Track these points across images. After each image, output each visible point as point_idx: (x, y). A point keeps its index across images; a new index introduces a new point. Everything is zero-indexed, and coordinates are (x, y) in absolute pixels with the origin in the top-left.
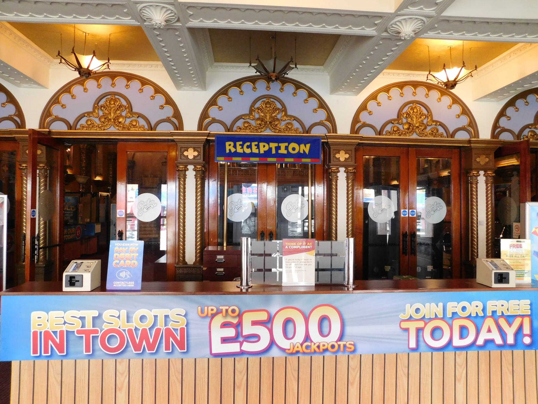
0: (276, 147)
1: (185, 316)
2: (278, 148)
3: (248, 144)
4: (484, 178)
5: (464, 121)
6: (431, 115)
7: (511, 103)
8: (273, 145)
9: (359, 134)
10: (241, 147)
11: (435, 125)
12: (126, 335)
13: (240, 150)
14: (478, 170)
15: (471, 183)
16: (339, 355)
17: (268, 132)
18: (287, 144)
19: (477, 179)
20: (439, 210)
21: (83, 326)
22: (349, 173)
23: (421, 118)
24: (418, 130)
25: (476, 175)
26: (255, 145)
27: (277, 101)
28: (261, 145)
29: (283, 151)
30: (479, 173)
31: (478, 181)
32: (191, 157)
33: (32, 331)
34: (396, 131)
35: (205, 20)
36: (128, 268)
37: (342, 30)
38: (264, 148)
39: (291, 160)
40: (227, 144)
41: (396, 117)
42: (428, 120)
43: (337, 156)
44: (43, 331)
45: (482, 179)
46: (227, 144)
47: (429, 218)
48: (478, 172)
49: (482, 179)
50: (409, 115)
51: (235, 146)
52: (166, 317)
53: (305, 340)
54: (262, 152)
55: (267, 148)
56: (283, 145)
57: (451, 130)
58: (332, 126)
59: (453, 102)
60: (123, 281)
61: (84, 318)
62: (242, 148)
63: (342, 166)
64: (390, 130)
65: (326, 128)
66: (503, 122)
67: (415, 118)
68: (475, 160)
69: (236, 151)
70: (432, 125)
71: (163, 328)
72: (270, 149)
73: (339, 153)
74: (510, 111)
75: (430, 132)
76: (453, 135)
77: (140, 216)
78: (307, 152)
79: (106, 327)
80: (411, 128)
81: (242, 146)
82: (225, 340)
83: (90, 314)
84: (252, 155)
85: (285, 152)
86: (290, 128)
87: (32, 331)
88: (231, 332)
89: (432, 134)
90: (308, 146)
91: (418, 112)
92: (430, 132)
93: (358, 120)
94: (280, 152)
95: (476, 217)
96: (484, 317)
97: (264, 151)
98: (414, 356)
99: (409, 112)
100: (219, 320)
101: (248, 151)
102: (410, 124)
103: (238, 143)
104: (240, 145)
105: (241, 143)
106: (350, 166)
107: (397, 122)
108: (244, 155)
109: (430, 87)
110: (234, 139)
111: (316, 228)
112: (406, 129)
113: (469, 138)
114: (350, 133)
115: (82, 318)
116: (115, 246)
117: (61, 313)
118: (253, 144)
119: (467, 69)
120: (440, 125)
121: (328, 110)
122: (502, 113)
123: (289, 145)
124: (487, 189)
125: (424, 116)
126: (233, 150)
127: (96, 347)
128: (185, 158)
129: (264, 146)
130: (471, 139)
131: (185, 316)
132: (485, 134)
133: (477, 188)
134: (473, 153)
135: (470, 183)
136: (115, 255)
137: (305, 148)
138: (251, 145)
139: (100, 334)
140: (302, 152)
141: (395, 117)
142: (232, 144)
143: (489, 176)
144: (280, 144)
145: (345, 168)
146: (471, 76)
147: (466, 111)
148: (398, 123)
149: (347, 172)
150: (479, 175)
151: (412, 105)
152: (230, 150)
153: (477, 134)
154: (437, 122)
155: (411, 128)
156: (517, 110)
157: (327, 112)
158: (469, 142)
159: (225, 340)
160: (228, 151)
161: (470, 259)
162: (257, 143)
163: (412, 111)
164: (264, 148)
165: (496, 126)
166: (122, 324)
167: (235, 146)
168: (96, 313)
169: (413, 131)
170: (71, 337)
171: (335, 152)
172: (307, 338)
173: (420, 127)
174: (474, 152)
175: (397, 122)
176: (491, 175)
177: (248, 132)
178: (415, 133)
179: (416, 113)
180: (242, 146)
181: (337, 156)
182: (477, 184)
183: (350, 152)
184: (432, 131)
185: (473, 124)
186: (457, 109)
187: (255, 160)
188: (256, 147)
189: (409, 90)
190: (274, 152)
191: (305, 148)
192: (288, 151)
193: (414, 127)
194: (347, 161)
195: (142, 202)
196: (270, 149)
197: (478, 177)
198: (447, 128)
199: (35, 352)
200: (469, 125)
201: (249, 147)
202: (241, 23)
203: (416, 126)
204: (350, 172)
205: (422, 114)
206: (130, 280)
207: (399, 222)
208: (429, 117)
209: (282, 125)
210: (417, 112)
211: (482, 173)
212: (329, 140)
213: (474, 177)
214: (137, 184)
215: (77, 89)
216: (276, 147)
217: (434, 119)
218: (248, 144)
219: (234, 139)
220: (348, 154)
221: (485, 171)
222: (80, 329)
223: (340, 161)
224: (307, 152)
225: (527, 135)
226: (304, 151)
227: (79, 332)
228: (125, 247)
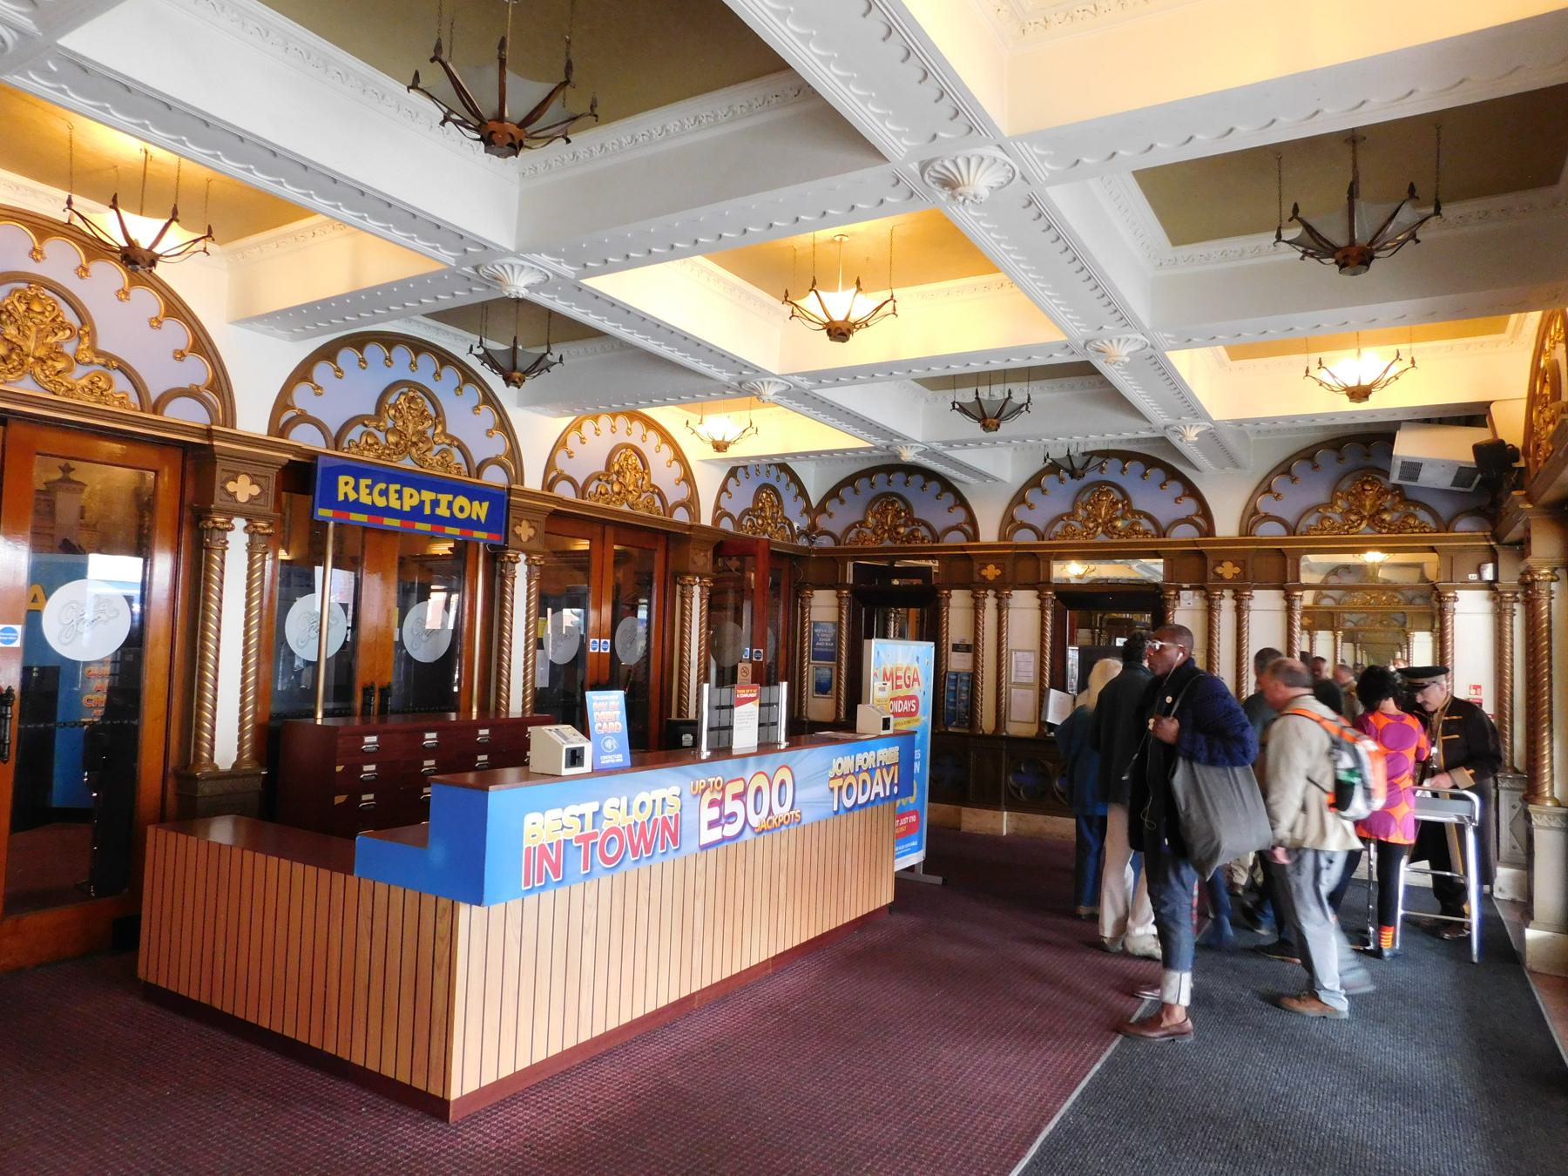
0: (432, 501)
1: (680, 797)
2: (435, 503)
3: (382, 486)
4: (246, 538)
5: (196, 372)
6: (92, 334)
7: (327, 353)
8: (428, 496)
9: (287, 439)
10: (368, 491)
11: (449, 445)
12: (625, 834)
13: (365, 499)
14: (230, 514)
15: (209, 549)
16: (791, 827)
17: (407, 464)
18: (450, 497)
19: (224, 538)
20: (105, 622)
21: (582, 830)
22: (257, 537)
23: (56, 334)
24: (43, 370)
25: (221, 527)
26: (396, 491)
27: (63, 299)
28: (407, 491)
29: (443, 511)
30: (233, 522)
31: (227, 542)
32: (242, 498)
33: (525, 847)
34: (371, 445)
35: (191, 143)
36: (613, 734)
37: (606, 326)
38: (411, 498)
39: (362, 518)
40: (342, 479)
41: (371, 411)
42: (82, 347)
43: (231, 486)
44: (537, 846)
45: (521, 569)
46: (342, 479)
47: (71, 642)
48: (229, 522)
49: (521, 569)
50: (400, 412)
51: (356, 489)
52: (664, 799)
53: (769, 815)
54: (407, 508)
55: (415, 502)
56: (444, 498)
57: (155, 392)
58: (224, 407)
59: (167, 310)
60: (611, 754)
61: (584, 815)
62: (371, 494)
63: (240, 514)
64: (357, 440)
65: (208, 409)
66: (303, 397)
67: (34, 329)
68: (224, 488)
69: (358, 499)
70: (91, 363)
71: (660, 817)
72: (422, 502)
73: (236, 481)
74: (322, 371)
75: (84, 382)
76: (157, 407)
77: (66, 644)
78: (483, 519)
79: (606, 826)
80: (14, 357)
81: (371, 488)
82: (712, 825)
83: (589, 808)
84: (389, 512)
85: (447, 514)
86: (105, 390)
87: (525, 847)
88: (714, 813)
89: (91, 390)
90: (486, 505)
91: (47, 314)
92: (84, 382)
93: (290, 403)
94: (439, 512)
95: (215, 642)
96: (875, 769)
97: (411, 507)
98: (837, 818)
99: (10, 307)
100: (708, 797)
101: (381, 502)
102: (401, 434)
103: (364, 482)
104: (367, 486)
105: (369, 482)
106: (261, 517)
107: (374, 424)
108: (371, 510)
109: (95, 248)
110: (358, 471)
111: (261, 675)
112: (393, 444)
113: (209, 422)
114: (266, 433)
115: (582, 817)
116: (593, 701)
117: (557, 813)
118: (394, 487)
119: (186, 227)
120: (119, 368)
121: (214, 360)
122: (303, 373)
123: (454, 497)
124: (529, 590)
125: (68, 332)
126: (352, 496)
127: (595, 861)
128: (229, 499)
129: (411, 496)
130: (214, 427)
131: (680, 797)
132: (253, 418)
133: (223, 562)
134: (218, 472)
135: (206, 549)
136: (595, 714)
137: (480, 510)
138: (387, 489)
139: (599, 840)
140: (474, 517)
141: (602, 468)
142: (352, 481)
143: (536, 565)
144: (440, 496)
145: (247, 520)
146: (205, 251)
147: (202, 345)
148: (377, 428)
149: (251, 531)
150: (232, 529)
151: (23, 286)
152: (346, 494)
153: (230, 416)
154: (453, 438)
155: (622, 495)
156: (156, 323)
157: (212, 365)
158: (209, 434)
159: (712, 825)
160: (341, 498)
161: (192, 761)
162: (398, 487)
163: (24, 307)
164: (411, 498)
165: (283, 401)
166: (621, 820)
167: (356, 489)
168: (595, 806)
169: (405, 451)
170: (570, 850)
171: (225, 475)
172: (770, 811)
173: (421, 445)
174: (220, 465)
175: (374, 424)
176: (262, 531)
177: (369, 456)
178: (408, 458)
179: (40, 317)
180: (371, 488)
181: (231, 486)
182: (513, 579)
183: (262, 481)
184: (93, 383)
185: (220, 384)
186: (177, 334)
187: (394, 523)
188: (397, 496)
189: (427, 363)
190: (427, 511)
191: (480, 510)
192: (452, 513)
193: (28, 355)
194: (256, 502)
195: (75, 605)
196: (422, 502)
197: (228, 533)
198: (145, 388)
199: (527, 883)
200: (210, 388)
201: (384, 493)
202: (304, 195)
203: (37, 355)
204: (262, 534)
205: (59, 325)
206: (616, 752)
207: (584, 660)
208: (86, 340)
209: (79, 376)
210: (42, 313)
211: (239, 523)
212: (215, 443)
213: (510, 564)
214: (314, 569)
215: (802, 503)
216: (432, 501)
217: (101, 346)
218: (382, 486)
219: (358, 471)
220: (259, 485)
221: (527, 555)
222: (579, 834)
223: (236, 501)
224: (483, 519)
225: (358, 441)
226: (478, 516)
227: (578, 839)
228: (605, 701)
